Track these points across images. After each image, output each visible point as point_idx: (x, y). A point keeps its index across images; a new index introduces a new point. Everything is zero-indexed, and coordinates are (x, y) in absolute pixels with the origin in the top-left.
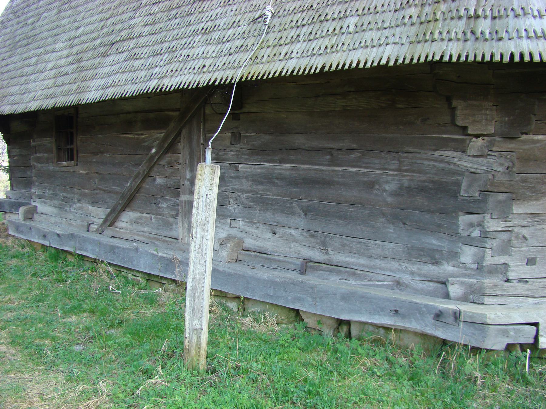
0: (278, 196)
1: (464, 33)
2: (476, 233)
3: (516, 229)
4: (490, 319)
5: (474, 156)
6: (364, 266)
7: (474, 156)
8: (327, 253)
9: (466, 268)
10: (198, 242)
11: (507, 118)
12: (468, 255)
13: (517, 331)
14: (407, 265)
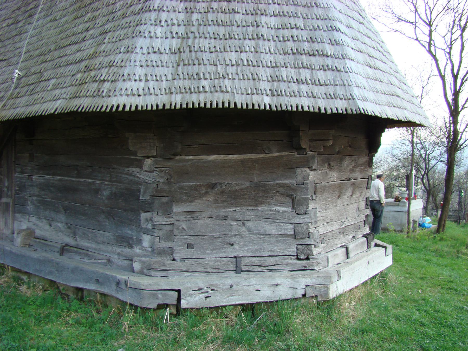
0: (52, 199)
2: (150, 226)
3: (176, 223)
4: (144, 286)
5: (147, 171)
6: (95, 249)
7: (147, 171)
8: (76, 240)
9: (146, 251)
11: (162, 145)
12: (146, 240)
13: (164, 295)
14: (116, 249)
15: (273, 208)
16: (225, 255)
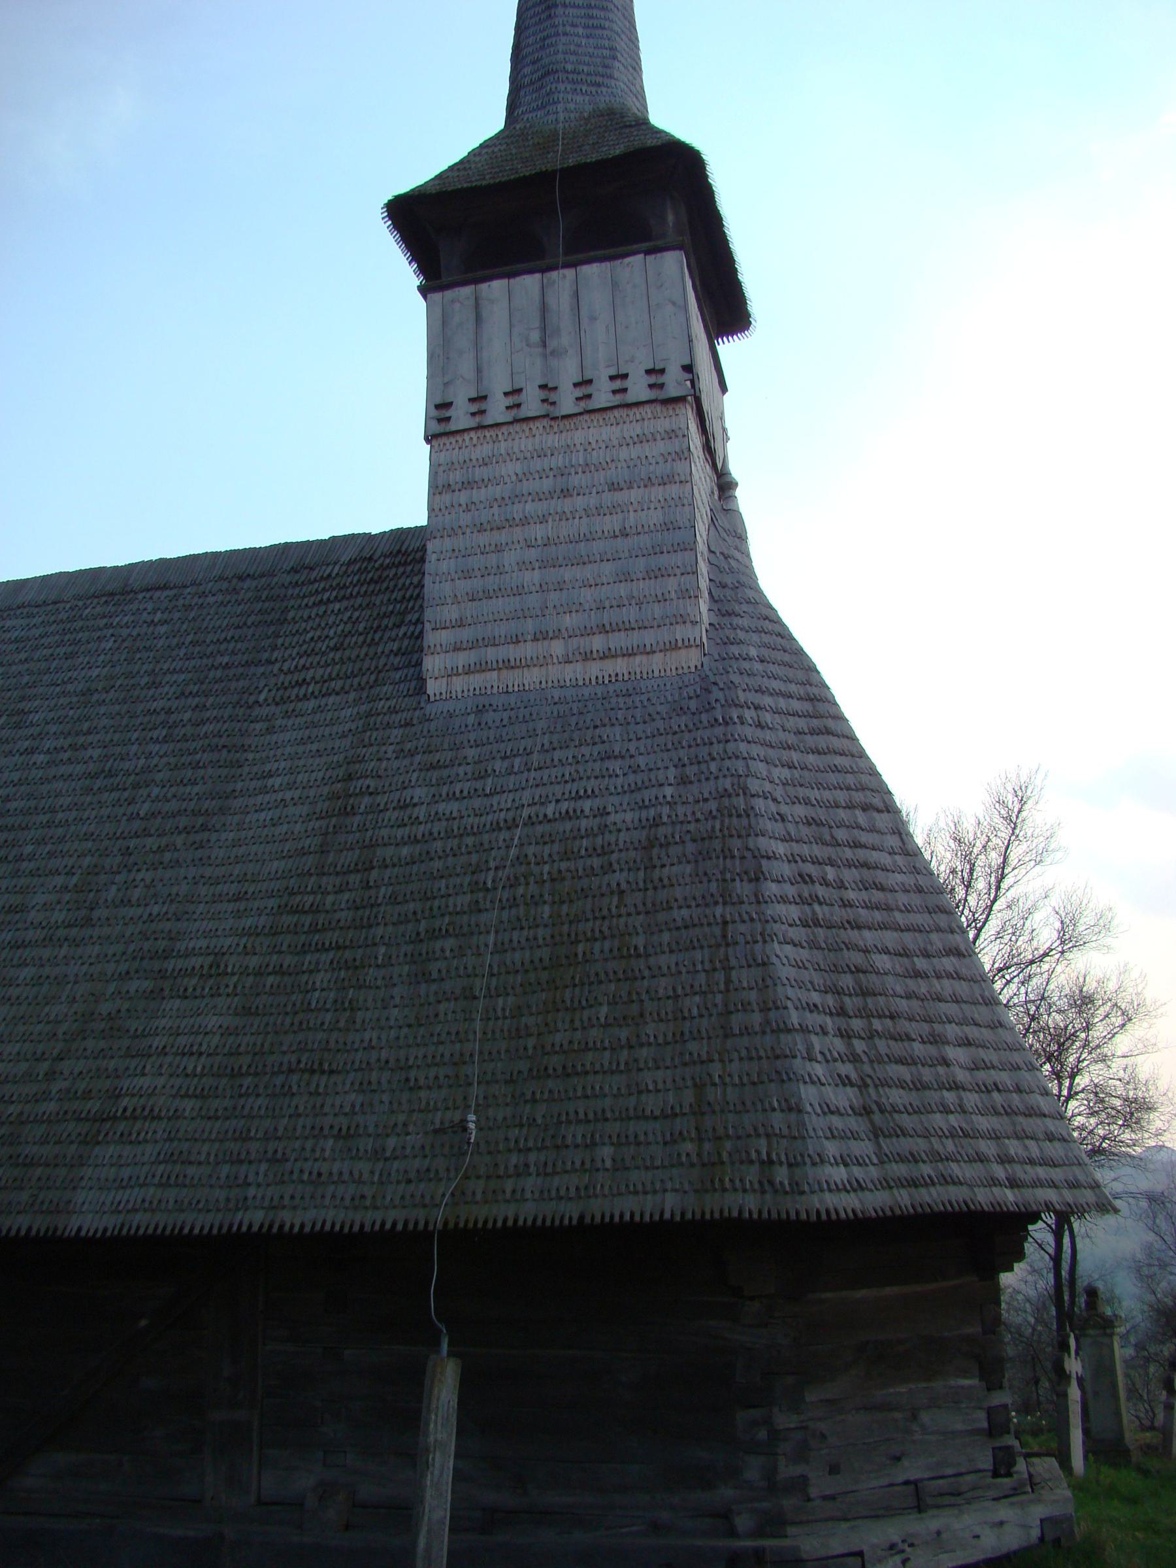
1: (760, 1183)
2: (762, 1434)
10: (436, 1472)
12: (753, 1470)
15: (952, 1382)
16: (886, 1481)
